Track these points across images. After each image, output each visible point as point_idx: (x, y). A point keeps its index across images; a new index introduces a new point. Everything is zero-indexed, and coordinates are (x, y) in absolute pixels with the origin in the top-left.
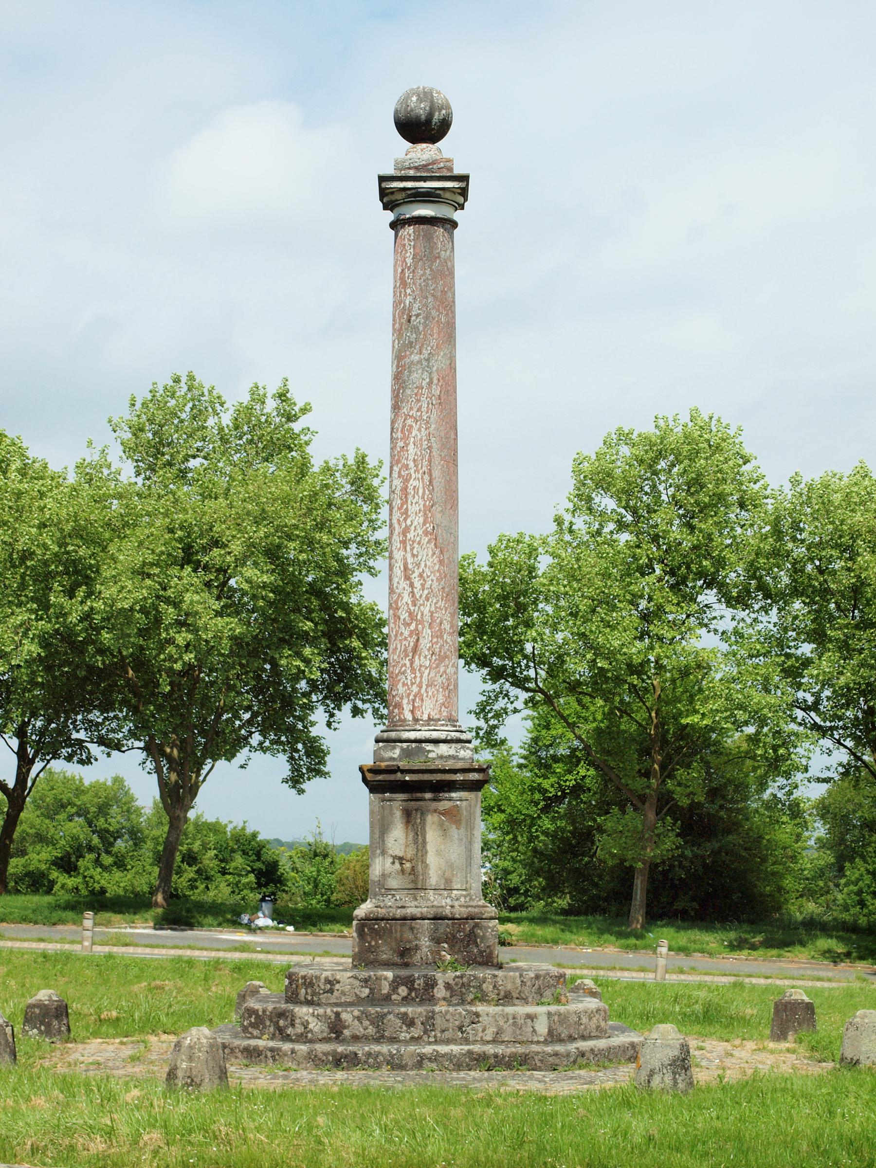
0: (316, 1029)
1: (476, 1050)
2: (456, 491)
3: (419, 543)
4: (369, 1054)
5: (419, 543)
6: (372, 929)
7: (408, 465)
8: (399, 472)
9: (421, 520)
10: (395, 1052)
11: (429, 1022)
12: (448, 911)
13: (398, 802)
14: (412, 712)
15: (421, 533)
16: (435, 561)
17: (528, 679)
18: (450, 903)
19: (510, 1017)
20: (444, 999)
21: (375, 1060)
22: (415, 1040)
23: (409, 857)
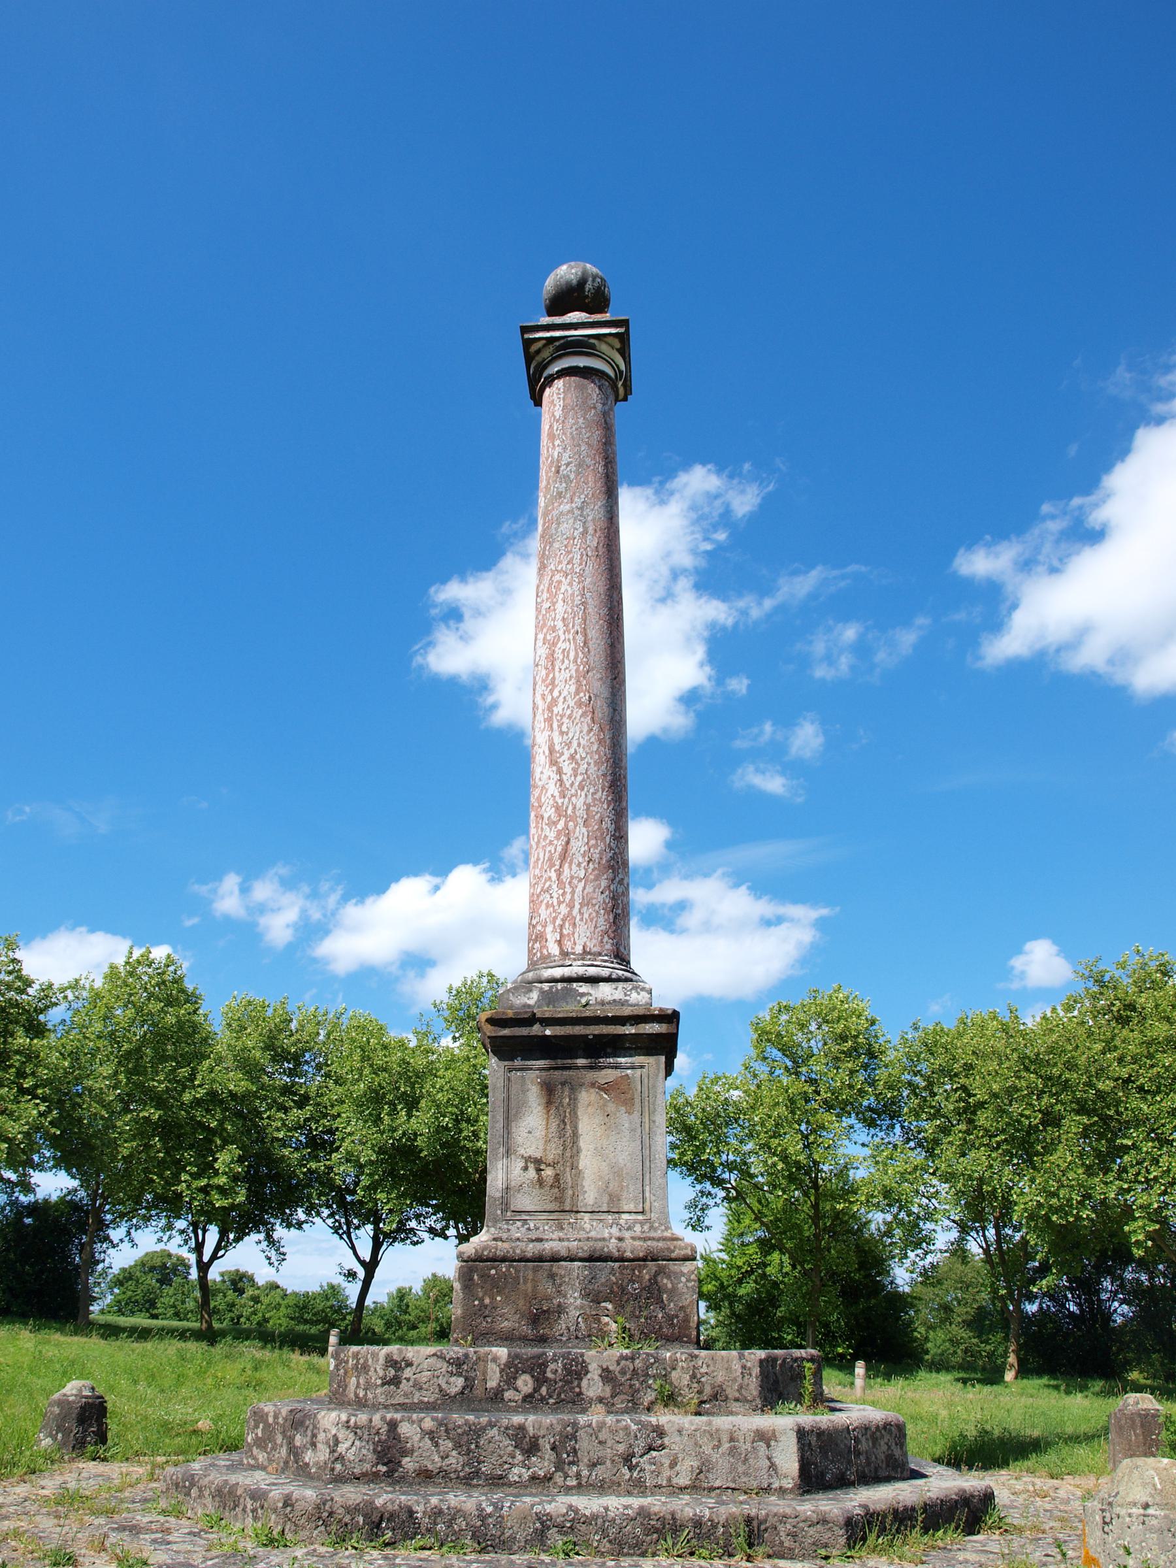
0: (350, 1455)
1: (656, 1509)
3: (570, 717)
4: (437, 1513)
5: (570, 717)
6: (484, 1276)
8: (544, 639)
9: (573, 689)
10: (489, 1509)
11: (565, 1446)
12: (612, 1246)
13: (531, 1078)
14: (560, 943)
15: (572, 703)
17: (724, 1181)
18: (618, 1234)
19: (725, 1438)
20: (601, 1400)
21: (450, 1525)
22: (540, 1482)
23: (550, 1158)
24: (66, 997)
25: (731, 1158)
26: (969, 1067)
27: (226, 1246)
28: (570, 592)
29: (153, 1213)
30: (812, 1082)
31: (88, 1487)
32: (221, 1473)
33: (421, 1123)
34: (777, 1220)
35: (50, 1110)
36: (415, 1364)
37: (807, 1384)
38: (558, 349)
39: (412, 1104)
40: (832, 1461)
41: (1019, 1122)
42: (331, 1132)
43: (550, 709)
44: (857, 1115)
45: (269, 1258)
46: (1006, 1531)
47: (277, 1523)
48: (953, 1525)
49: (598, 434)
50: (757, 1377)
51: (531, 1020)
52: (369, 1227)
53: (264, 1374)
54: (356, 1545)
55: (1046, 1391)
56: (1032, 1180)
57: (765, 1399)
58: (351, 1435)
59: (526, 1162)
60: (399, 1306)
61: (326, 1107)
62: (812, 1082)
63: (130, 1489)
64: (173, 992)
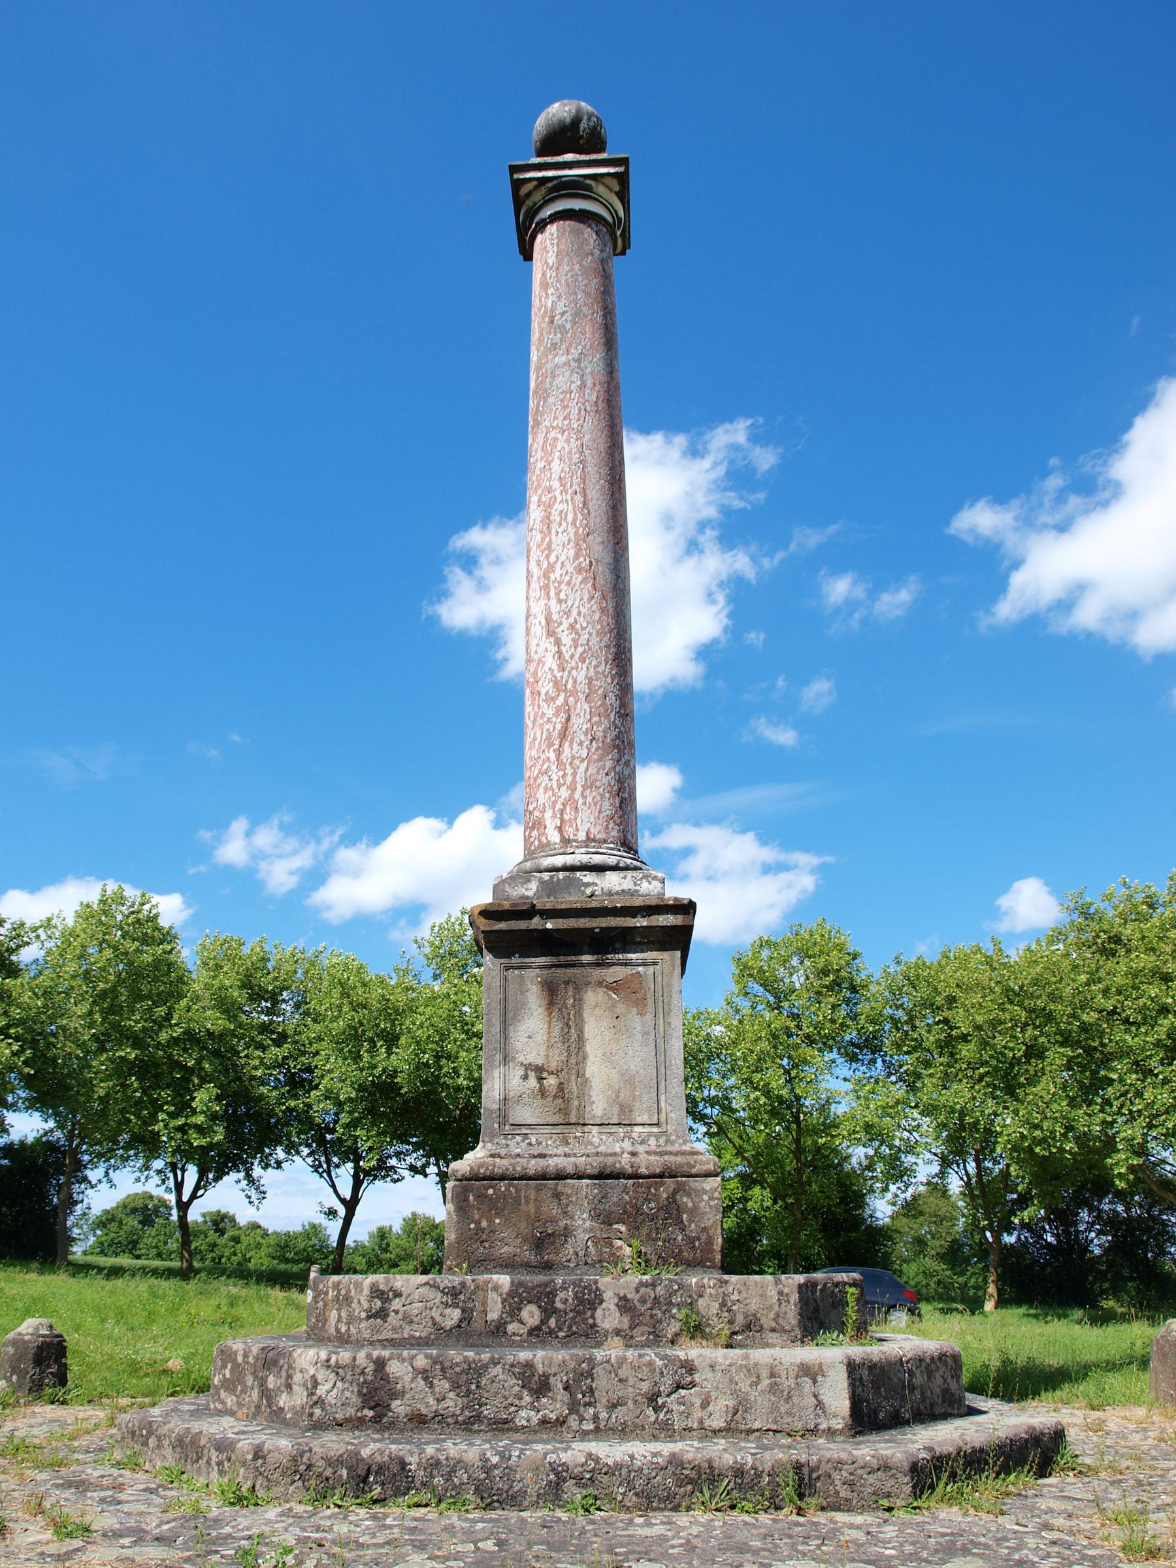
0: (331, 1399)
1: (689, 1456)
2: (627, 568)
5: (568, 583)
7: (551, 486)
9: (572, 553)
10: (495, 1459)
11: (580, 1385)
12: (625, 1162)
13: (531, 976)
14: (560, 829)
15: (571, 569)
16: (594, 608)
18: (631, 1149)
19: (765, 1373)
20: (618, 1332)
21: (449, 1477)
23: (553, 1065)
24: (38, 937)
25: (713, 1093)
26: (951, 1000)
27: (205, 1187)
28: (567, 449)
29: (132, 1152)
30: (795, 1017)
31: (39, 1434)
32: (183, 1420)
33: (401, 1059)
34: (759, 1154)
35: (22, 1050)
36: (405, 1295)
37: (849, 1311)
38: (551, 191)
39: (391, 1040)
40: (885, 1398)
41: (1002, 1053)
42: (309, 1069)
44: (839, 1049)
46: (1080, 1472)
47: (246, 1478)
48: (1027, 1467)
49: (595, 282)
50: (795, 1305)
51: (530, 912)
52: (350, 1166)
53: (241, 1310)
54: (339, 1502)
55: (1025, 1320)
56: (1016, 1112)
57: (805, 1329)
58: (332, 1376)
59: (526, 1069)
60: (380, 1246)
62: (795, 1017)
63: (87, 1437)
64: (148, 931)
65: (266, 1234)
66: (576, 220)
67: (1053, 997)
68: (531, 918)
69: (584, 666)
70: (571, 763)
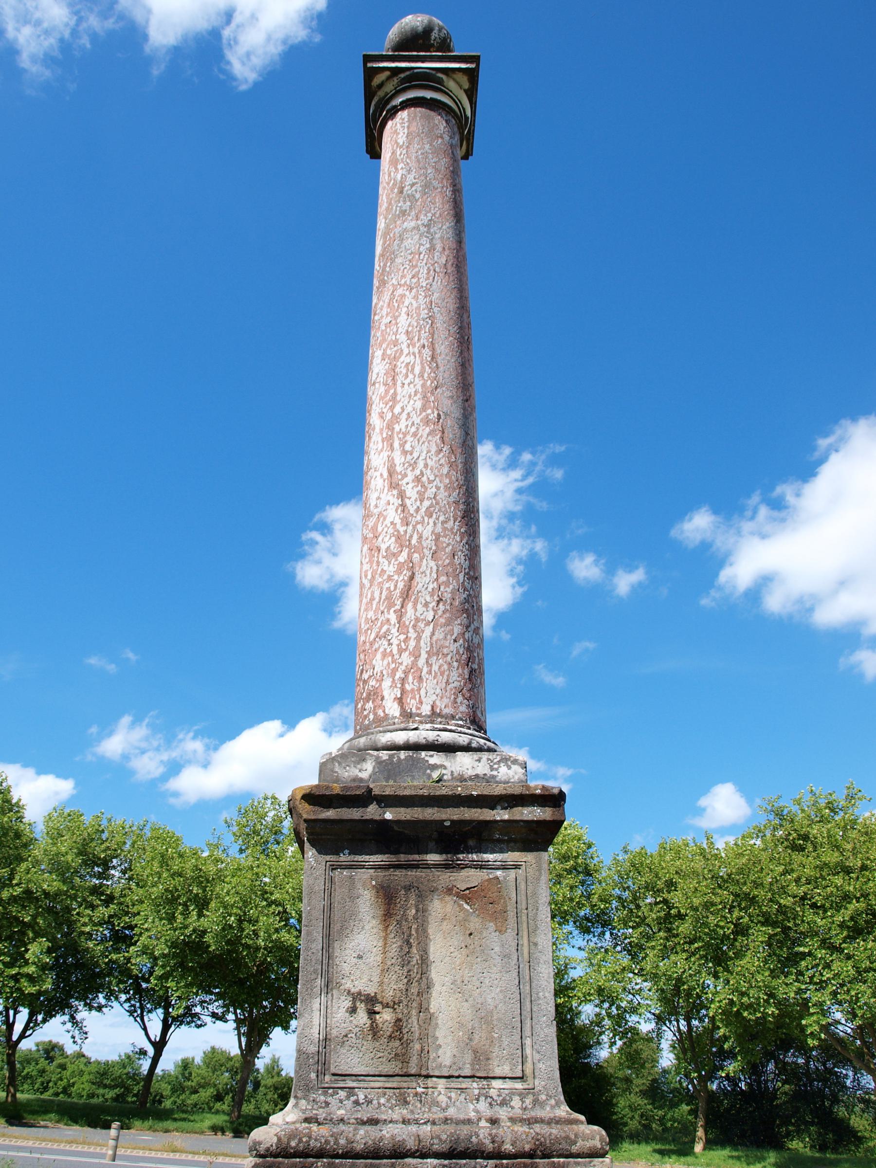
3: (415, 435)
5: (415, 435)
7: (397, 340)
9: (419, 405)
12: (483, 1133)
14: (400, 701)
16: (442, 461)
23: (389, 995)
28: (415, 305)
33: (211, 921)
38: (403, 81)
39: (202, 904)
42: (131, 927)
43: (390, 427)
44: (575, 923)
45: (73, 1037)
51: (365, 798)
52: (160, 1011)
55: (731, 1161)
59: (354, 1001)
60: (183, 1074)
61: (128, 906)
65: (89, 1062)
66: (427, 108)
67: (757, 885)
68: (365, 805)
69: (431, 521)
70: (414, 626)
